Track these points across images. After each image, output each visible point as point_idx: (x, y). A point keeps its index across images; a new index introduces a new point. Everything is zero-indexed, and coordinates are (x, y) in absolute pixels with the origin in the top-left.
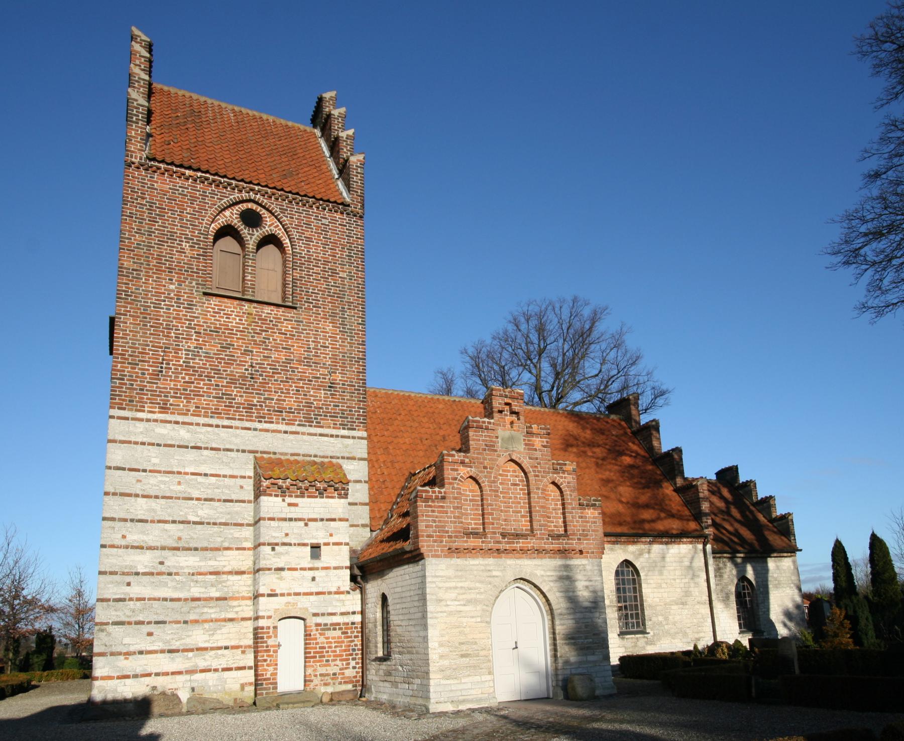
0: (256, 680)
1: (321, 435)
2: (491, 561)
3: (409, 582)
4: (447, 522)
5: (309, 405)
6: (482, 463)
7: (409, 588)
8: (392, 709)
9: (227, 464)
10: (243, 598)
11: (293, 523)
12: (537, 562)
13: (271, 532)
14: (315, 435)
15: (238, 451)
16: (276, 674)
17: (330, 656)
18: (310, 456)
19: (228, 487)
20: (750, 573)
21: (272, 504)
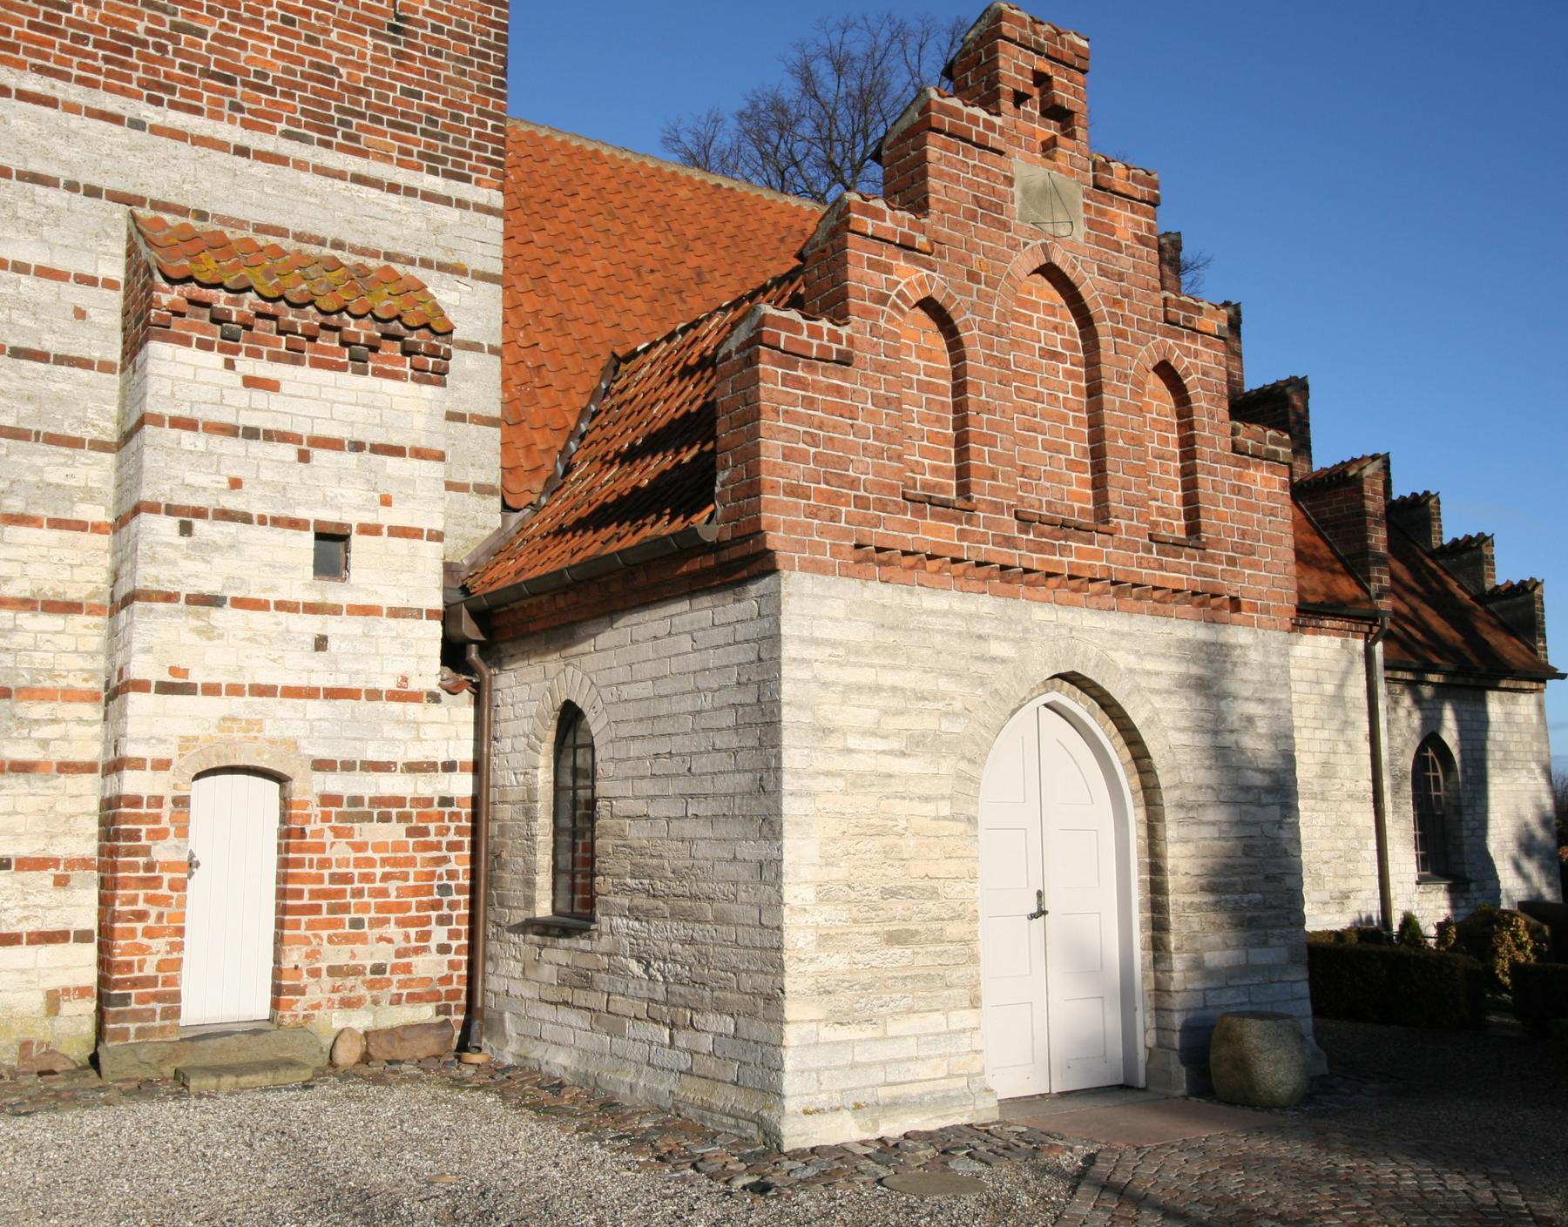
0: (103, 981)
1: (359, 179)
2: (985, 604)
3: (694, 661)
4: (852, 448)
5: (324, 74)
6: (962, 260)
7: (688, 683)
8: (594, 1109)
9: (33, 227)
10: (70, 695)
11: (258, 447)
12: (1116, 622)
13: (179, 468)
14: (341, 175)
15: (72, 187)
16: (177, 965)
17: (365, 908)
18: (321, 242)
19: (32, 308)
20: (1450, 734)
21: (184, 372)
